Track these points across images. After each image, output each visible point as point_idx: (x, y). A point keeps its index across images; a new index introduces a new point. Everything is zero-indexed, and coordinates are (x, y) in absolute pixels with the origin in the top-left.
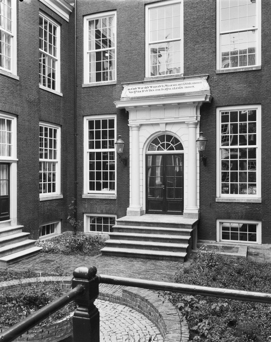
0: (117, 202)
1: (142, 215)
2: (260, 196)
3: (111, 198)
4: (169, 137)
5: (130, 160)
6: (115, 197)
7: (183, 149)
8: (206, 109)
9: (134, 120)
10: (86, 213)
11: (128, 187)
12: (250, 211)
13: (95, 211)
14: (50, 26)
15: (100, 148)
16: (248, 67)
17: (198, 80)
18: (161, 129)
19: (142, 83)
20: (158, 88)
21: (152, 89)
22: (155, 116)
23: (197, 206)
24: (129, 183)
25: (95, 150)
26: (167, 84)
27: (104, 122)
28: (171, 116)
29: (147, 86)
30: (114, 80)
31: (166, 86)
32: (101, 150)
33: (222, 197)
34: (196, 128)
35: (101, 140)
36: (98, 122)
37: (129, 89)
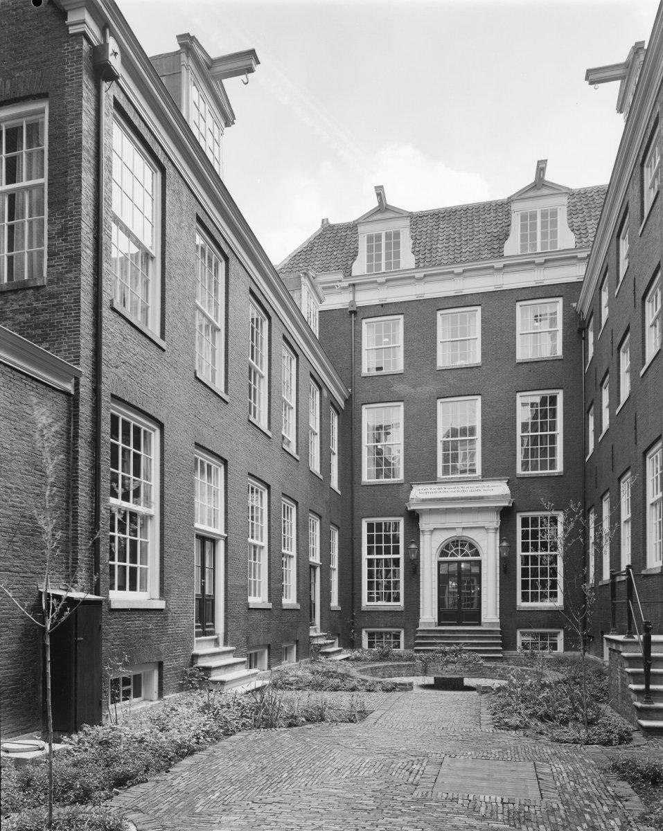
0: (404, 614)
1: (542, 161)
3: (398, 610)
5: (421, 566)
7: (479, 556)
8: (506, 514)
9: (425, 523)
10: (366, 627)
11: (419, 597)
12: (553, 619)
15: (382, 554)
18: (458, 533)
19: (435, 483)
21: (446, 490)
22: (451, 521)
24: (419, 593)
25: (375, 556)
28: (468, 521)
29: (440, 487)
30: (401, 477)
31: (462, 487)
32: (383, 556)
33: (521, 604)
34: (496, 533)
35: (383, 545)
36: (379, 525)
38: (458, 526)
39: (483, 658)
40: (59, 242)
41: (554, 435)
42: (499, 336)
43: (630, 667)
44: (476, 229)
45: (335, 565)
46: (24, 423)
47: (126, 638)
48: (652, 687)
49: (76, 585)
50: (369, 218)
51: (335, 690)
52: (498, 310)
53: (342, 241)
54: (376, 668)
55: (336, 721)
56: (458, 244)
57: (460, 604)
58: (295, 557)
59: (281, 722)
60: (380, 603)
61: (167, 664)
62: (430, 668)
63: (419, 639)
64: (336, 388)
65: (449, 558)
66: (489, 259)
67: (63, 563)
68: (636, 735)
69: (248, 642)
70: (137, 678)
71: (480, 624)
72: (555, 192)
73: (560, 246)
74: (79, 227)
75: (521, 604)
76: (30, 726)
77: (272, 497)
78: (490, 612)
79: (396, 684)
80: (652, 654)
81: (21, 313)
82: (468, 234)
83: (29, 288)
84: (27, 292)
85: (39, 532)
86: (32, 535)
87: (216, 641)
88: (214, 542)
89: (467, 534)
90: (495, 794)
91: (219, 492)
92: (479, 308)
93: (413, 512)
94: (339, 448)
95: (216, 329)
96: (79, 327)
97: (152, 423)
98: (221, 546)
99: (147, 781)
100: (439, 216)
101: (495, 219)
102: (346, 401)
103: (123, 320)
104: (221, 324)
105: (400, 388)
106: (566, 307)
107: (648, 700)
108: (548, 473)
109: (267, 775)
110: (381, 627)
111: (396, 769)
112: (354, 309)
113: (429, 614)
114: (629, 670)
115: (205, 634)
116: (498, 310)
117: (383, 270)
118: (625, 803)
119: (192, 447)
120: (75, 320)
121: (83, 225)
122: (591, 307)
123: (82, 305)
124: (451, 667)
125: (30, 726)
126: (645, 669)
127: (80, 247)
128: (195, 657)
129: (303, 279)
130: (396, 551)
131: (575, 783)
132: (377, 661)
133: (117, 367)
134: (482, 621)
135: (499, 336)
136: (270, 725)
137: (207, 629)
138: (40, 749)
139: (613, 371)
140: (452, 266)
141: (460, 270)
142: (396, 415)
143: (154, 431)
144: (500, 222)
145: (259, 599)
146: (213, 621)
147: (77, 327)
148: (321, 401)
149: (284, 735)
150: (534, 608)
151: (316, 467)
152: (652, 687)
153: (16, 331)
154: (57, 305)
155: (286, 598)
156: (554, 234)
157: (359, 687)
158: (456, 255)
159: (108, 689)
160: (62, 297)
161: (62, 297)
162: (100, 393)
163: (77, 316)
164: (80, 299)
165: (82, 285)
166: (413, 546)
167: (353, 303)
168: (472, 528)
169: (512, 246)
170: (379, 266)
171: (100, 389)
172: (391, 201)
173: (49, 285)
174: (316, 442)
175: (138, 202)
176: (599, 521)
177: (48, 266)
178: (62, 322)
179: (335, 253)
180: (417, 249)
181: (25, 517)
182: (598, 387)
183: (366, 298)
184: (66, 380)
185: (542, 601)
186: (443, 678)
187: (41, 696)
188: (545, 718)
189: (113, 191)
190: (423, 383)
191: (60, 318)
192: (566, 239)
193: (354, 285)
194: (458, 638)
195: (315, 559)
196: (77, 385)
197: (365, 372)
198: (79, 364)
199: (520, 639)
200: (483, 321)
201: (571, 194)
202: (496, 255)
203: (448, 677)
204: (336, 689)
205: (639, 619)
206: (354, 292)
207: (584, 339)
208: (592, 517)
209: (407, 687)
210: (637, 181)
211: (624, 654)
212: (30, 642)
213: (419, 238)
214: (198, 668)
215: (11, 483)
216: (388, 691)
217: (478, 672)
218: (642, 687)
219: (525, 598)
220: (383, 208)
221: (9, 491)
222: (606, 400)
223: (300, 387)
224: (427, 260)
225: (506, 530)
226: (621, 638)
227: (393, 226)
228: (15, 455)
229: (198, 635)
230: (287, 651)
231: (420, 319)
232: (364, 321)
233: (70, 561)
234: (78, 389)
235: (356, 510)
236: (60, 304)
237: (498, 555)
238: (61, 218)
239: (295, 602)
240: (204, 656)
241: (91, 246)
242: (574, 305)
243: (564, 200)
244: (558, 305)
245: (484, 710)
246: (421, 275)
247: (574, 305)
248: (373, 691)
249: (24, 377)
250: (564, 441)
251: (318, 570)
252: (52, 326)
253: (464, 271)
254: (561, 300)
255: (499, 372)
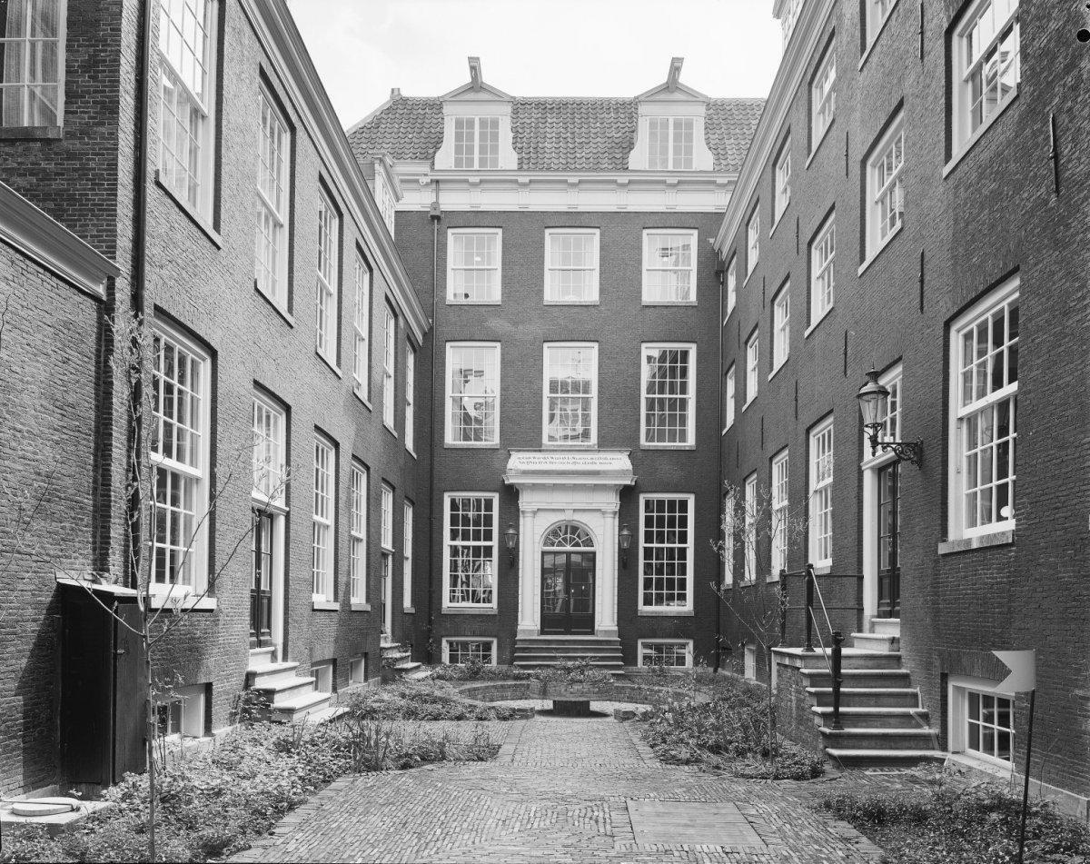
0: (498, 618)
1: (678, 59)
2: (692, 608)
4: (575, 529)
6: (495, 611)
8: (627, 495)
9: (526, 502)
10: (447, 636)
12: (680, 627)
13: (463, 633)
14: (169, 349)
16: (678, 444)
17: (618, 455)
18: (568, 516)
19: (540, 451)
20: (561, 460)
22: (560, 500)
23: (613, 620)
25: (482, 543)
26: (575, 456)
27: (672, 503)
28: (581, 500)
30: (494, 440)
32: (472, 543)
33: (644, 609)
34: (614, 518)
36: (661, 503)
37: (519, 458)
38: (567, 507)
39: (613, 675)
40: (83, 79)
41: (685, 399)
42: (620, 268)
43: (812, 686)
44: (593, 131)
45: (408, 552)
46: (40, 336)
47: (168, 650)
48: (842, 709)
49: (106, 574)
50: (458, 96)
51: (436, 719)
52: (622, 238)
53: (419, 121)
54: (475, 689)
55: (460, 759)
56: (571, 146)
57: (570, 610)
58: (365, 542)
59: (389, 763)
60: (465, 604)
61: (216, 688)
62: (551, 690)
63: (514, 650)
64: (413, 316)
65: (555, 548)
66: (610, 170)
67: (88, 542)
68: (827, 767)
69: (311, 656)
70: (177, 709)
71: (592, 633)
72: (690, 98)
73: (696, 166)
74: (116, 62)
75: (644, 609)
76: (44, 778)
77: (341, 459)
78: (606, 617)
79: (514, 710)
80: (842, 671)
81: (20, 175)
82: (583, 134)
83: (36, 140)
84: (32, 144)
85: (57, 496)
86: (49, 501)
87: (274, 654)
88: (271, 517)
89: (578, 517)
90: (713, 844)
91: (201, 440)
92: (597, 231)
93: (511, 487)
94: (415, 397)
95: (278, 225)
96: (116, 205)
97: (202, 348)
98: (281, 521)
99: (250, 847)
100: (543, 106)
101: (615, 121)
102: (425, 335)
103: (170, 201)
104: (283, 218)
105: (496, 324)
106: (702, 242)
107: (838, 725)
108: (677, 446)
109: (415, 833)
110: (467, 636)
111: (576, 817)
112: (438, 213)
113: (529, 619)
114: (813, 690)
115: (260, 644)
116: (622, 238)
117: (476, 167)
118: (857, 846)
119: (251, 386)
120: (108, 195)
121: (123, 61)
122: (734, 245)
123: (120, 174)
124: (577, 687)
125: (44, 778)
126: (834, 688)
127: (118, 91)
128: (250, 677)
129: (377, 166)
130: (488, 536)
131: (791, 825)
132: (466, 680)
133: (161, 267)
134: (596, 628)
135: (620, 268)
136: (373, 766)
137: (262, 638)
138: (73, 810)
139: (764, 325)
140: (566, 174)
141: (575, 180)
142: (489, 359)
143: (204, 360)
144: (622, 126)
145: (324, 598)
146: (269, 627)
147: (112, 205)
148: (396, 333)
149: (393, 779)
150: (652, 613)
151: (389, 421)
152: (842, 709)
153: (49, 211)
154: (79, 169)
155: (317, 592)
156: (689, 151)
157: (468, 715)
158: (569, 160)
159: (154, 719)
160: (89, 159)
161: (89, 159)
162: (142, 302)
163: (112, 190)
164: (116, 165)
165: (120, 146)
166: (511, 531)
167: (436, 205)
168: (584, 510)
169: (639, 159)
170: (470, 162)
171: (142, 297)
172: (487, 78)
173: (66, 139)
174: (389, 387)
175: (189, 37)
176: (740, 508)
177: (66, 112)
178: (87, 195)
179: (410, 136)
180: (519, 146)
181: (39, 474)
182: (742, 345)
183: (453, 201)
184: (97, 280)
185: (668, 605)
186: (566, 702)
187: (59, 734)
188: (716, 749)
189: (161, 20)
190: (523, 323)
191: (85, 190)
192: (703, 159)
193: (437, 182)
194: (568, 650)
195: (387, 544)
196: (111, 288)
197: (450, 298)
198: (115, 258)
199: (641, 651)
200: (602, 249)
201: (709, 104)
202: (618, 167)
203: (573, 700)
204: (436, 718)
205: (823, 627)
206: (437, 191)
207: (722, 283)
208: (730, 505)
209: (525, 714)
210: (804, 101)
211: (803, 671)
212: (46, 656)
213: (520, 131)
214: (258, 690)
215: (22, 424)
216: (505, 719)
217: (606, 694)
218: (830, 709)
219: (648, 602)
220: (476, 86)
221: (19, 435)
222: (752, 362)
223: (374, 312)
224: (533, 161)
225: (626, 515)
226: (798, 651)
227: (490, 111)
228: (27, 382)
229: (252, 646)
230: (353, 667)
231: (523, 237)
232: (450, 231)
233: (98, 539)
234: (113, 294)
235: (428, 476)
236: (84, 170)
237: (617, 546)
238: (87, 46)
239: (364, 601)
240: (262, 674)
241: (132, 92)
242: (712, 240)
243: (702, 110)
244: (693, 238)
245: (636, 740)
246: (526, 180)
247: (712, 240)
248: (485, 719)
249: (41, 270)
250: (697, 408)
251: (390, 558)
252: (72, 199)
253: (580, 182)
254: (695, 232)
255: (615, 318)
